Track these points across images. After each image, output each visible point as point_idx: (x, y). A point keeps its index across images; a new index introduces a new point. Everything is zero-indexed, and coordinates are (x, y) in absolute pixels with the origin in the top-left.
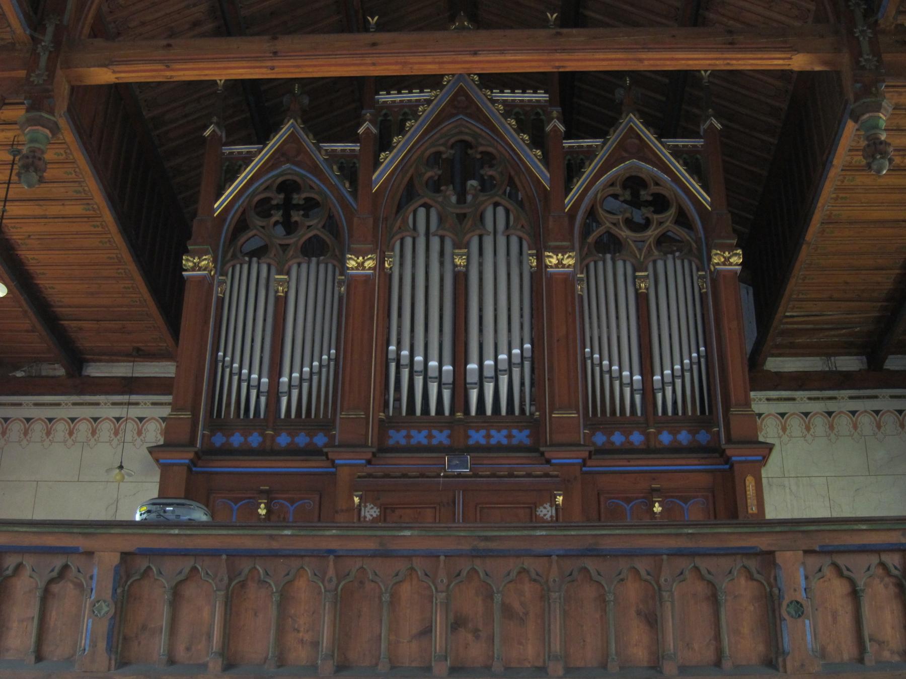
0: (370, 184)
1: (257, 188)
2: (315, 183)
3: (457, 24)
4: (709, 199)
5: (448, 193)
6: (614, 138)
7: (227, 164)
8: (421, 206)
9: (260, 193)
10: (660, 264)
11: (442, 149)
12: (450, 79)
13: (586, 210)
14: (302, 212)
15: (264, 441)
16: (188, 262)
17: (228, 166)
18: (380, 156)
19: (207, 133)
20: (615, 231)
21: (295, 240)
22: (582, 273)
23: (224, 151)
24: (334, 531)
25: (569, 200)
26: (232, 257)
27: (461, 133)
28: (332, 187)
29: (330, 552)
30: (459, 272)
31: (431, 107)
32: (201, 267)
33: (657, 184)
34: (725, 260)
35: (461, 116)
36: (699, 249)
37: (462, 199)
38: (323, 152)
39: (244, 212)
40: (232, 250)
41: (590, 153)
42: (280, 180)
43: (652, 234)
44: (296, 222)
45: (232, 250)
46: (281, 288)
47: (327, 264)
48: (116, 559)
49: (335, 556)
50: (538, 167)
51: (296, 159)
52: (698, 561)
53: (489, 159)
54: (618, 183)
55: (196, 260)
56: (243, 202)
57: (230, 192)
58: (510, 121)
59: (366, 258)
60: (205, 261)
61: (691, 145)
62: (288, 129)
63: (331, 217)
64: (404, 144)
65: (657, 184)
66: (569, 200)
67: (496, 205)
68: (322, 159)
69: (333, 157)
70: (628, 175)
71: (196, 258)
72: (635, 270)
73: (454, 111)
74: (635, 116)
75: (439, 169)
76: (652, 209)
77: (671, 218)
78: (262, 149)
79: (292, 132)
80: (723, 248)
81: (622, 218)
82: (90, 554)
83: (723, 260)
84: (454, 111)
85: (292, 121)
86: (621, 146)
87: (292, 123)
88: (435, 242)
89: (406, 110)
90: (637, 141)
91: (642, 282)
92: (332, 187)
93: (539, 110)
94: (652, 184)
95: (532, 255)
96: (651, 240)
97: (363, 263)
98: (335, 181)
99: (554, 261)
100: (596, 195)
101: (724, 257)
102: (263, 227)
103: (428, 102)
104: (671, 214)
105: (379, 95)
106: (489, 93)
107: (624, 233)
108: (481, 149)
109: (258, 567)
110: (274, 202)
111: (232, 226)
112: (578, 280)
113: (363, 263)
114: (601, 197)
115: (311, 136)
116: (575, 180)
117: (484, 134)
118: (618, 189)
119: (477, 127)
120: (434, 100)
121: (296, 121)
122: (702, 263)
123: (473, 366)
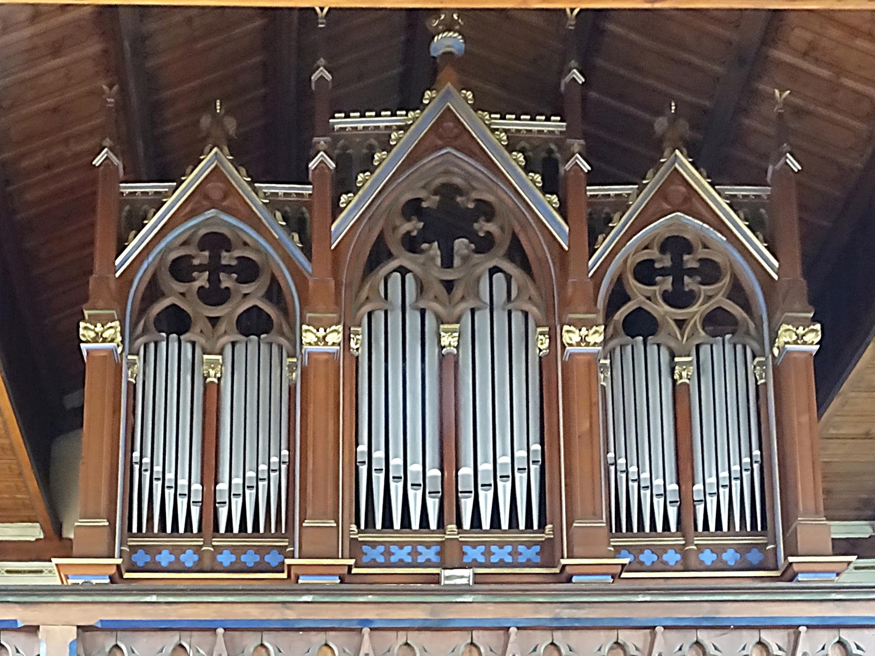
0: (329, 235)
1: (171, 242)
2: (251, 237)
3: (443, 17)
4: (776, 264)
5: (432, 252)
6: (653, 182)
7: (127, 208)
8: (395, 270)
9: (176, 248)
10: (705, 350)
11: (422, 194)
12: (434, 96)
13: (612, 279)
14: (235, 276)
15: (200, 560)
16: (86, 331)
17: (130, 211)
18: (340, 200)
19: (97, 161)
20: (649, 306)
21: (227, 311)
22: (605, 358)
23: (122, 190)
24: (370, 597)
25: (595, 262)
26: (143, 331)
27: (447, 172)
28: (276, 244)
29: (366, 622)
30: (449, 354)
31: (408, 133)
32: (106, 338)
33: (705, 247)
34: (798, 338)
35: (448, 150)
36: (759, 328)
37: (447, 262)
38: (261, 195)
39: (154, 275)
40: (142, 323)
41: (621, 204)
42: (203, 232)
43: (697, 311)
44: (227, 288)
45: (142, 323)
46: (212, 373)
47: (271, 344)
48: (72, 633)
49: (371, 629)
50: (554, 218)
51: (224, 204)
52: (845, 634)
53: (486, 210)
54: (655, 244)
55: (99, 328)
56: (154, 259)
57: (135, 245)
58: (516, 156)
59: (328, 330)
60: (112, 330)
61: (753, 195)
62: (210, 162)
63: (274, 279)
64: (356, 205)
65: (705, 247)
66: (595, 262)
67: (494, 270)
68: (261, 203)
69: (273, 203)
70: (667, 235)
71: (99, 325)
72: (673, 356)
73: (440, 143)
74: (682, 152)
75: (420, 220)
76: (699, 279)
77: (724, 289)
78: (177, 188)
79: (216, 167)
80: (796, 322)
81: (660, 289)
82: (33, 630)
83: (795, 337)
84: (440, 143)
85: (215, 149)
86: (662, 193)
87: (216, 153)
88: (414, 319)
89: (373, 141)
90: (682, 189)
91: (684, 370)
92: (276, 244)
93: (553, 147)
94: (700, 247)
95: (542, 333)
96: (697, 317)
97: (324, 337)
98: (278, 233)
99: (576, 338)
100: (625, 261)
101: (797, 335)
102: (183, 294)
103: (405, 128)
104: (724, 284)
105: (334, 118)
106: (487, 117)
107: (661, 310)
108: (475, 195)
109: (266, 644)
110: (196, 262)
111: (140, 296)
112: (601, 367)
113: (324, 337)
114: (632, 262)
115: (243, 171)
116: (600, 238)
117: (480, 175)
118: (654, 253)
119: (471, 165)
120: (411, 124)
121: (221, 150)
122: (762, 345)
123: (466, 471)
